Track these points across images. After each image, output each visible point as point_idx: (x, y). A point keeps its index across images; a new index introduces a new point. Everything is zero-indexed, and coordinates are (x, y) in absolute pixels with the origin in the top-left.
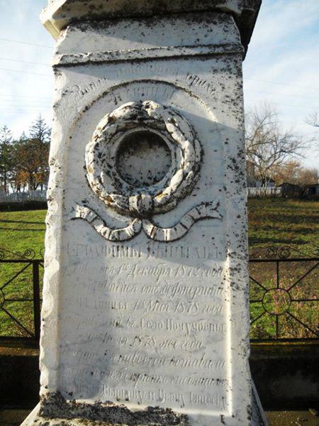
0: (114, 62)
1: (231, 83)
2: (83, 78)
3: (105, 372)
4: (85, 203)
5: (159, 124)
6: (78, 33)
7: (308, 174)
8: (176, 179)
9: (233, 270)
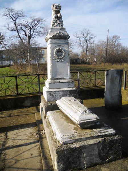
0: (56, 43)
1: (68, 46)
2: (53, 45)
3: (57, 75)
4: (54, 58)
5: (61, 50)
6: (52, 40)
7: (123, 50)
8: (63, 55)
9: (69, 64)
